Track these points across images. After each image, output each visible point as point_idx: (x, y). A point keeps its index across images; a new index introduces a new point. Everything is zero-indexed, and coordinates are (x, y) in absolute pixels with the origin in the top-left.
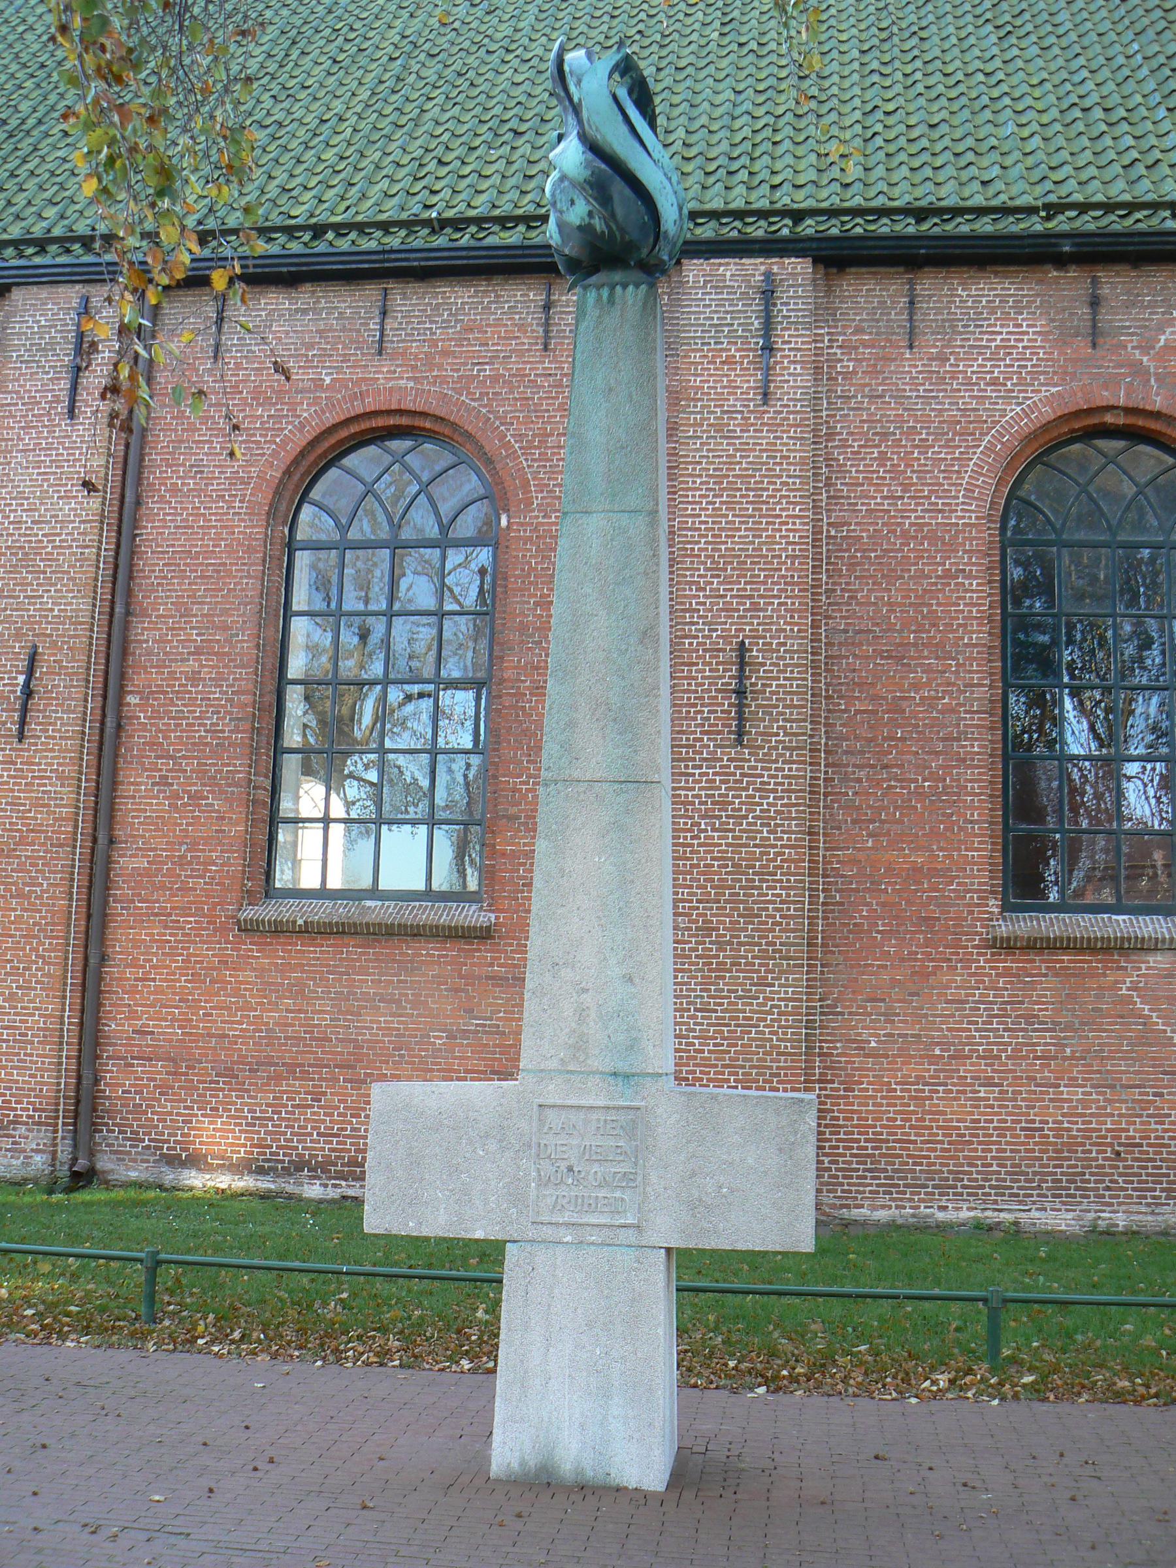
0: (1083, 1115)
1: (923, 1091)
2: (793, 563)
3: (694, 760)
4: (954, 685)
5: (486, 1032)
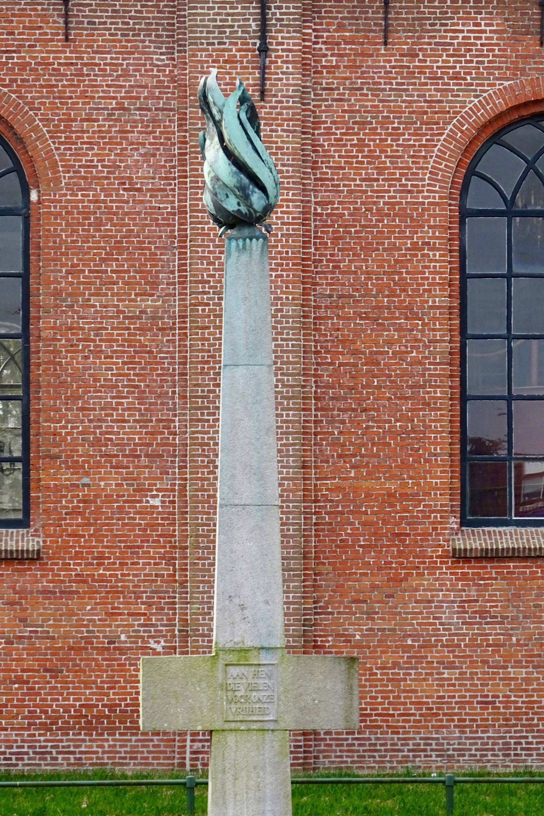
0: (526, 690)
1: (399, 674)
2: (287, 241)
3: (208, 408)
4: (420, 341)
5: (37, 638)
